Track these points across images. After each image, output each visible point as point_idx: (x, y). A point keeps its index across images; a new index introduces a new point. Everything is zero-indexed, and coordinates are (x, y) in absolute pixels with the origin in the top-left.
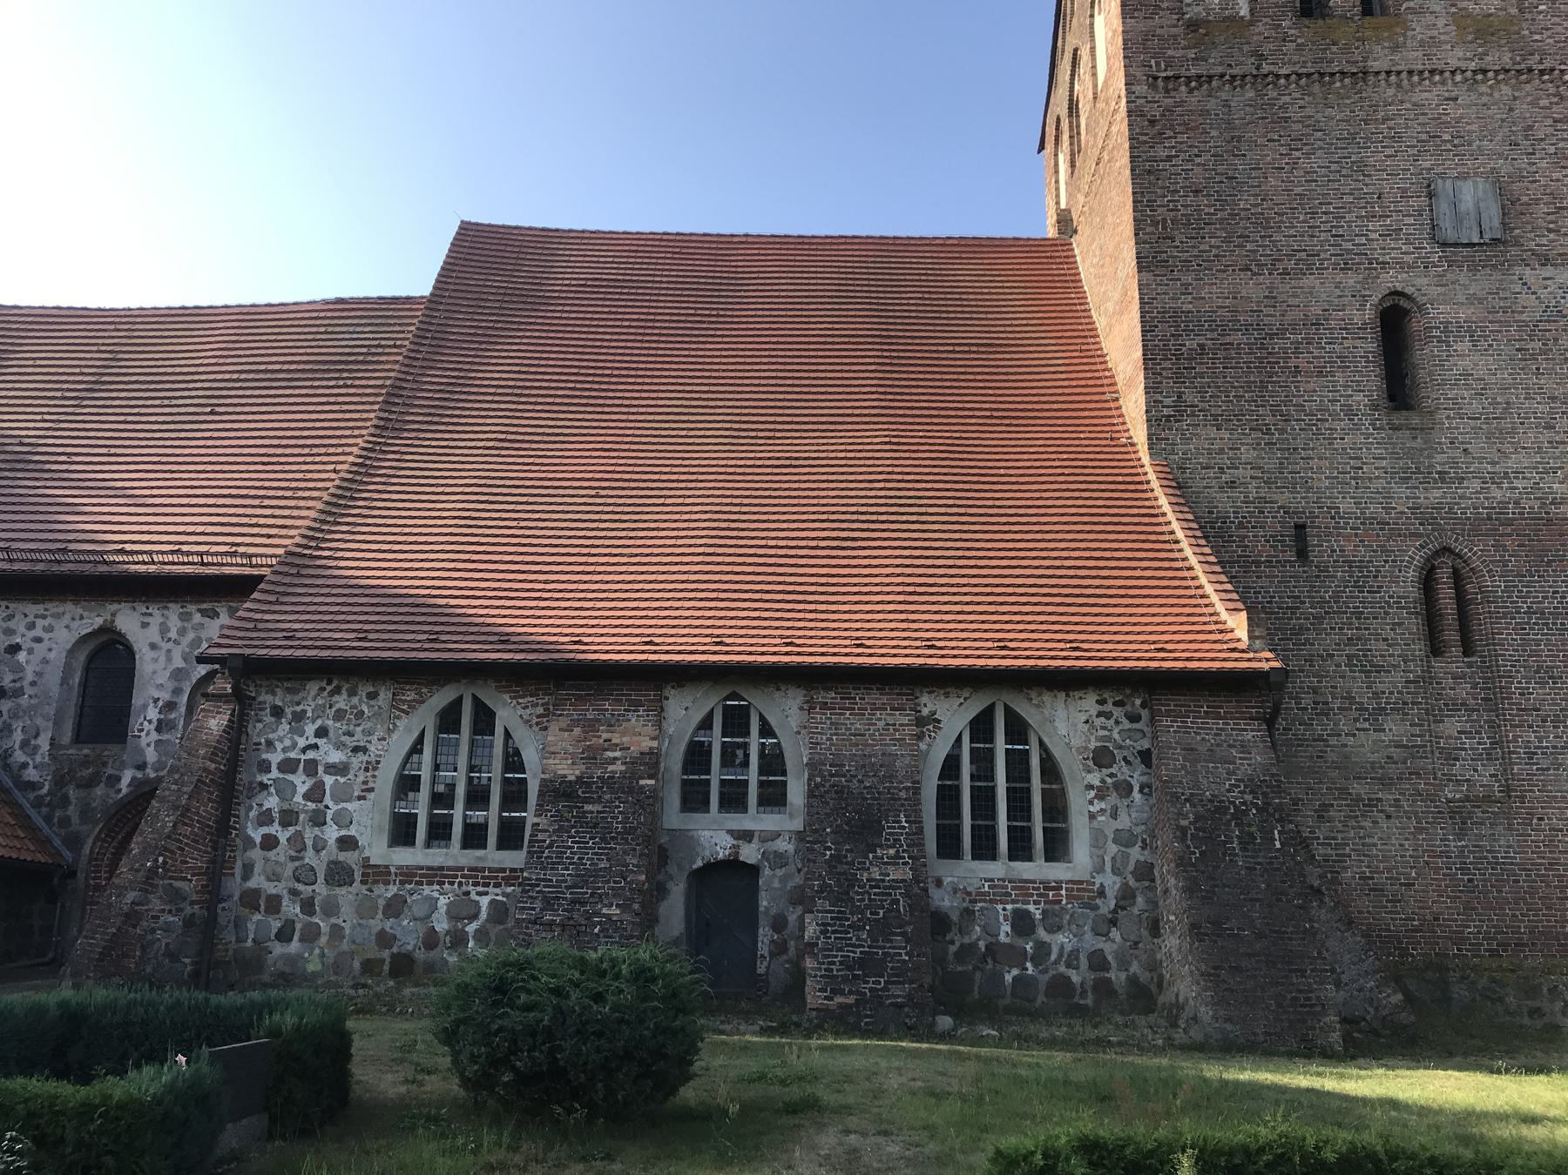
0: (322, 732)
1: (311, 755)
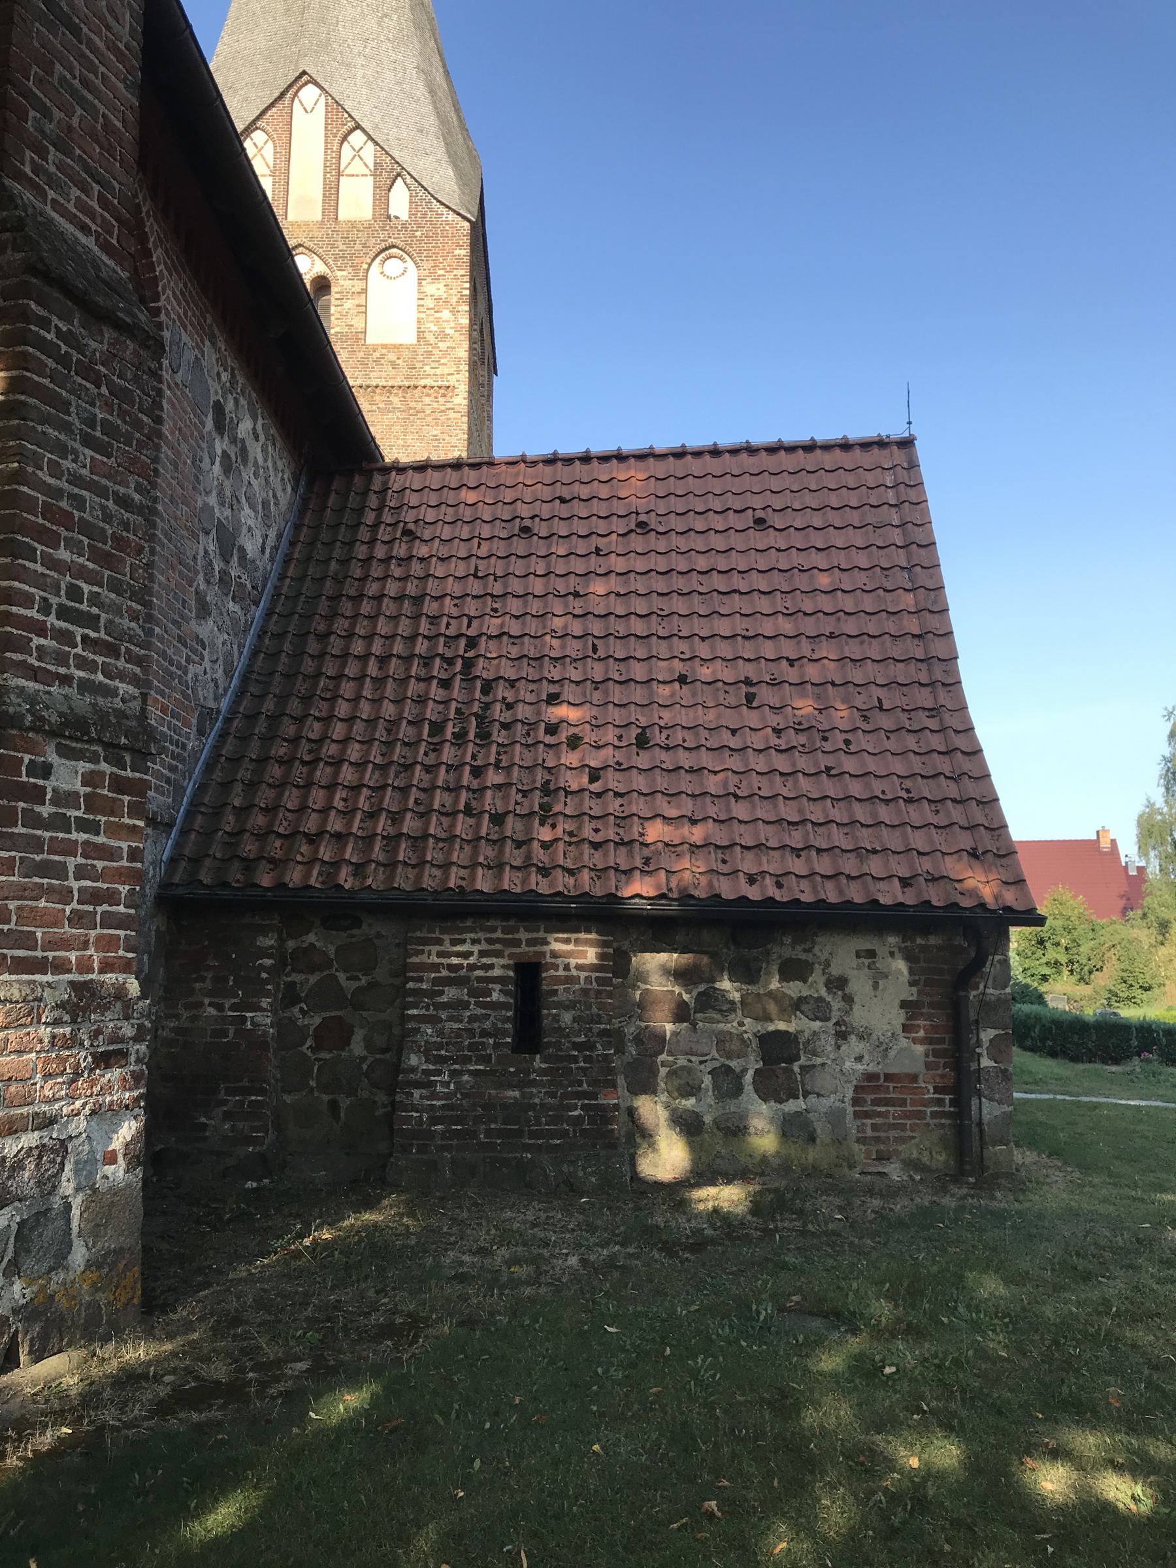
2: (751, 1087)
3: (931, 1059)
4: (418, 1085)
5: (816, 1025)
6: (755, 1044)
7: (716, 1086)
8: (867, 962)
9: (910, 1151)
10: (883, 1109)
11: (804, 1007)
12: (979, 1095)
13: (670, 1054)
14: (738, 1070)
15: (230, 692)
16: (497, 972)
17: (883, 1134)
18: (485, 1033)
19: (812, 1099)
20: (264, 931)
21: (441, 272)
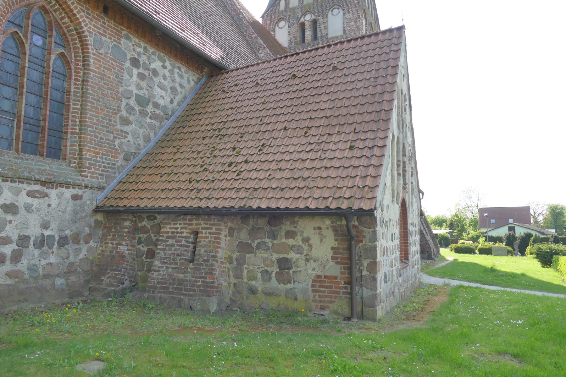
2: (275, 278)
3: (343, 270)
4: (156, 271)
5: (298, 256)
6: (276, 262)
7: (263, 278)
8: (318, 231)
9: (334, 306)
10: (323, 289)
11: (293, 249)
12: (361, 286)
13: (248, 265)
14: (270, 272)
15: (146, 148)
16: (184, 234)
17: (323, 299)
18: (178, 255)
19: (296, 284)
20: (125, 220)
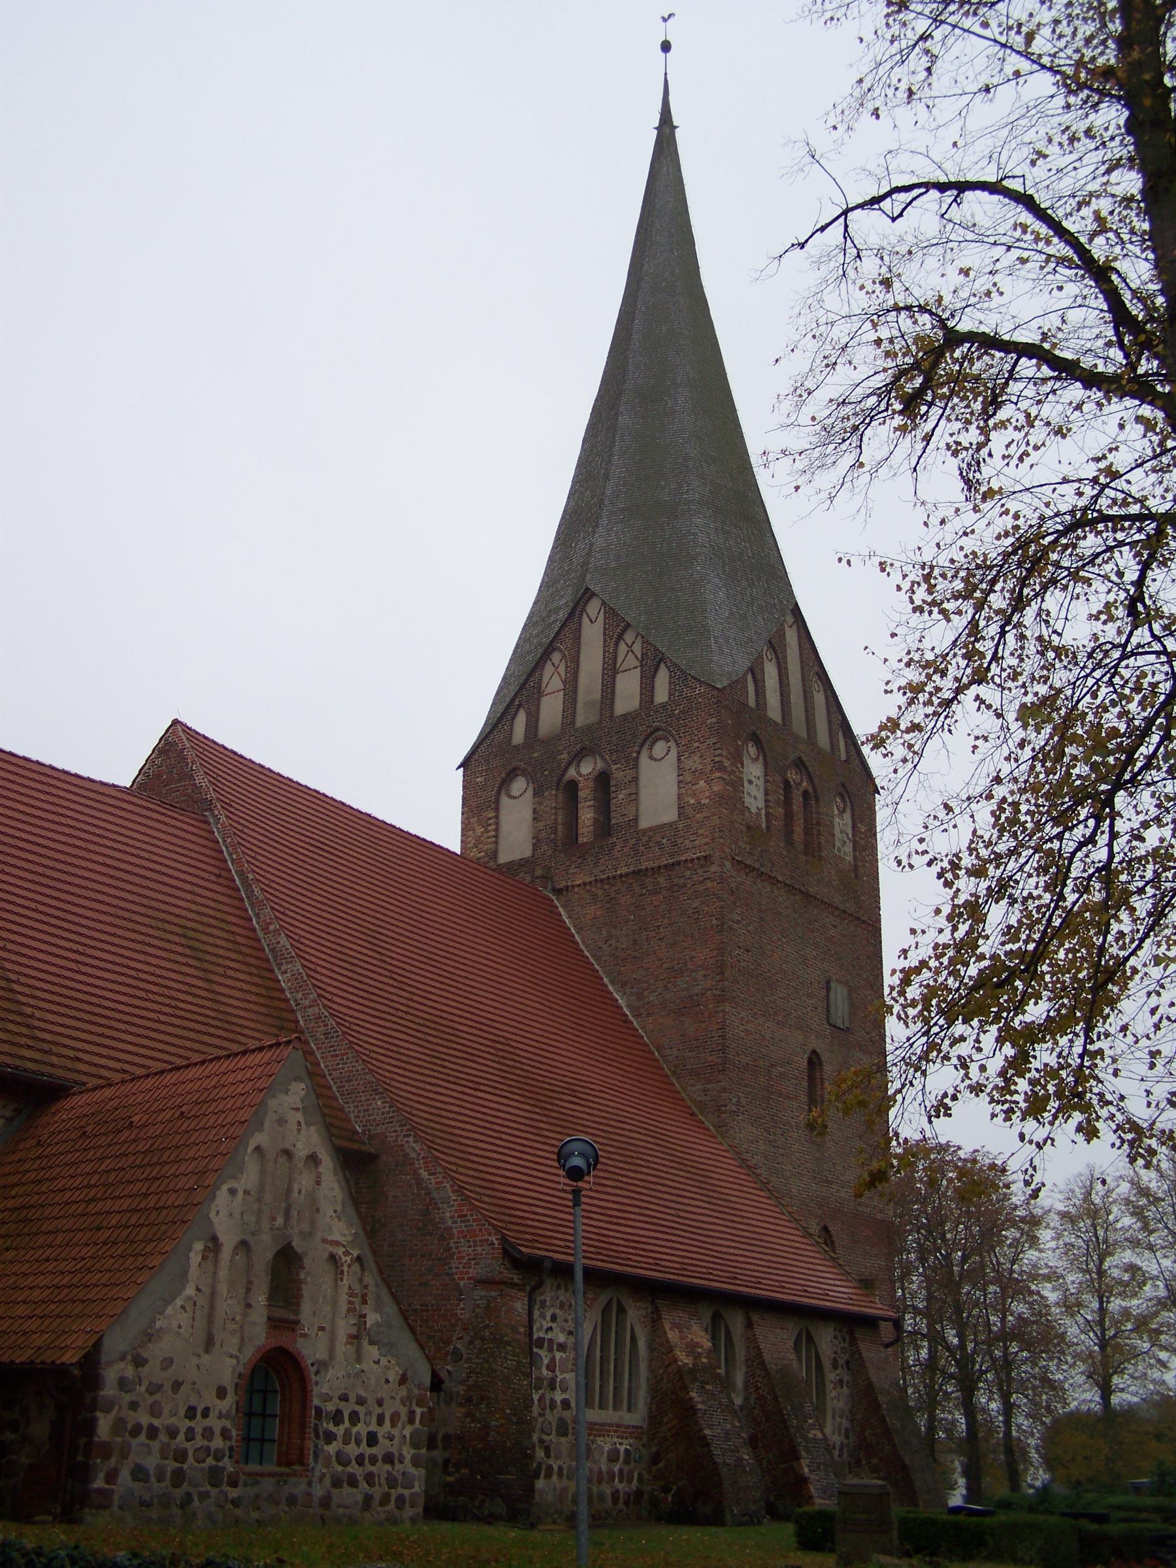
0: (554, 1318)
1: (549, 1336)
21: (696, 744)
